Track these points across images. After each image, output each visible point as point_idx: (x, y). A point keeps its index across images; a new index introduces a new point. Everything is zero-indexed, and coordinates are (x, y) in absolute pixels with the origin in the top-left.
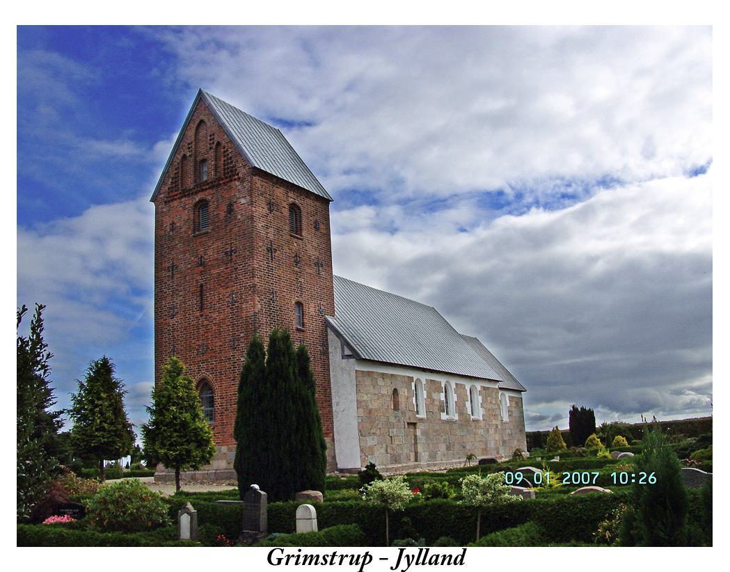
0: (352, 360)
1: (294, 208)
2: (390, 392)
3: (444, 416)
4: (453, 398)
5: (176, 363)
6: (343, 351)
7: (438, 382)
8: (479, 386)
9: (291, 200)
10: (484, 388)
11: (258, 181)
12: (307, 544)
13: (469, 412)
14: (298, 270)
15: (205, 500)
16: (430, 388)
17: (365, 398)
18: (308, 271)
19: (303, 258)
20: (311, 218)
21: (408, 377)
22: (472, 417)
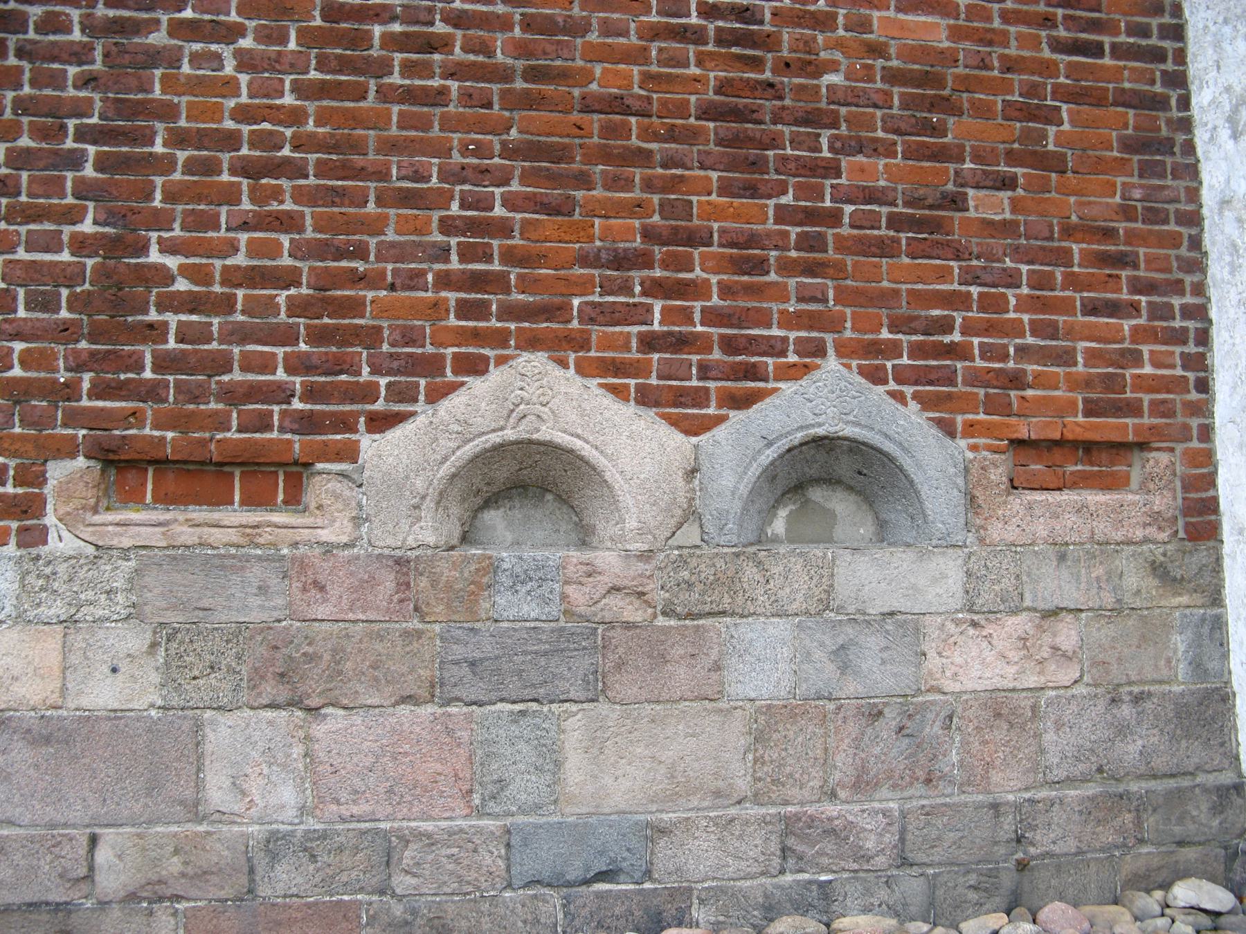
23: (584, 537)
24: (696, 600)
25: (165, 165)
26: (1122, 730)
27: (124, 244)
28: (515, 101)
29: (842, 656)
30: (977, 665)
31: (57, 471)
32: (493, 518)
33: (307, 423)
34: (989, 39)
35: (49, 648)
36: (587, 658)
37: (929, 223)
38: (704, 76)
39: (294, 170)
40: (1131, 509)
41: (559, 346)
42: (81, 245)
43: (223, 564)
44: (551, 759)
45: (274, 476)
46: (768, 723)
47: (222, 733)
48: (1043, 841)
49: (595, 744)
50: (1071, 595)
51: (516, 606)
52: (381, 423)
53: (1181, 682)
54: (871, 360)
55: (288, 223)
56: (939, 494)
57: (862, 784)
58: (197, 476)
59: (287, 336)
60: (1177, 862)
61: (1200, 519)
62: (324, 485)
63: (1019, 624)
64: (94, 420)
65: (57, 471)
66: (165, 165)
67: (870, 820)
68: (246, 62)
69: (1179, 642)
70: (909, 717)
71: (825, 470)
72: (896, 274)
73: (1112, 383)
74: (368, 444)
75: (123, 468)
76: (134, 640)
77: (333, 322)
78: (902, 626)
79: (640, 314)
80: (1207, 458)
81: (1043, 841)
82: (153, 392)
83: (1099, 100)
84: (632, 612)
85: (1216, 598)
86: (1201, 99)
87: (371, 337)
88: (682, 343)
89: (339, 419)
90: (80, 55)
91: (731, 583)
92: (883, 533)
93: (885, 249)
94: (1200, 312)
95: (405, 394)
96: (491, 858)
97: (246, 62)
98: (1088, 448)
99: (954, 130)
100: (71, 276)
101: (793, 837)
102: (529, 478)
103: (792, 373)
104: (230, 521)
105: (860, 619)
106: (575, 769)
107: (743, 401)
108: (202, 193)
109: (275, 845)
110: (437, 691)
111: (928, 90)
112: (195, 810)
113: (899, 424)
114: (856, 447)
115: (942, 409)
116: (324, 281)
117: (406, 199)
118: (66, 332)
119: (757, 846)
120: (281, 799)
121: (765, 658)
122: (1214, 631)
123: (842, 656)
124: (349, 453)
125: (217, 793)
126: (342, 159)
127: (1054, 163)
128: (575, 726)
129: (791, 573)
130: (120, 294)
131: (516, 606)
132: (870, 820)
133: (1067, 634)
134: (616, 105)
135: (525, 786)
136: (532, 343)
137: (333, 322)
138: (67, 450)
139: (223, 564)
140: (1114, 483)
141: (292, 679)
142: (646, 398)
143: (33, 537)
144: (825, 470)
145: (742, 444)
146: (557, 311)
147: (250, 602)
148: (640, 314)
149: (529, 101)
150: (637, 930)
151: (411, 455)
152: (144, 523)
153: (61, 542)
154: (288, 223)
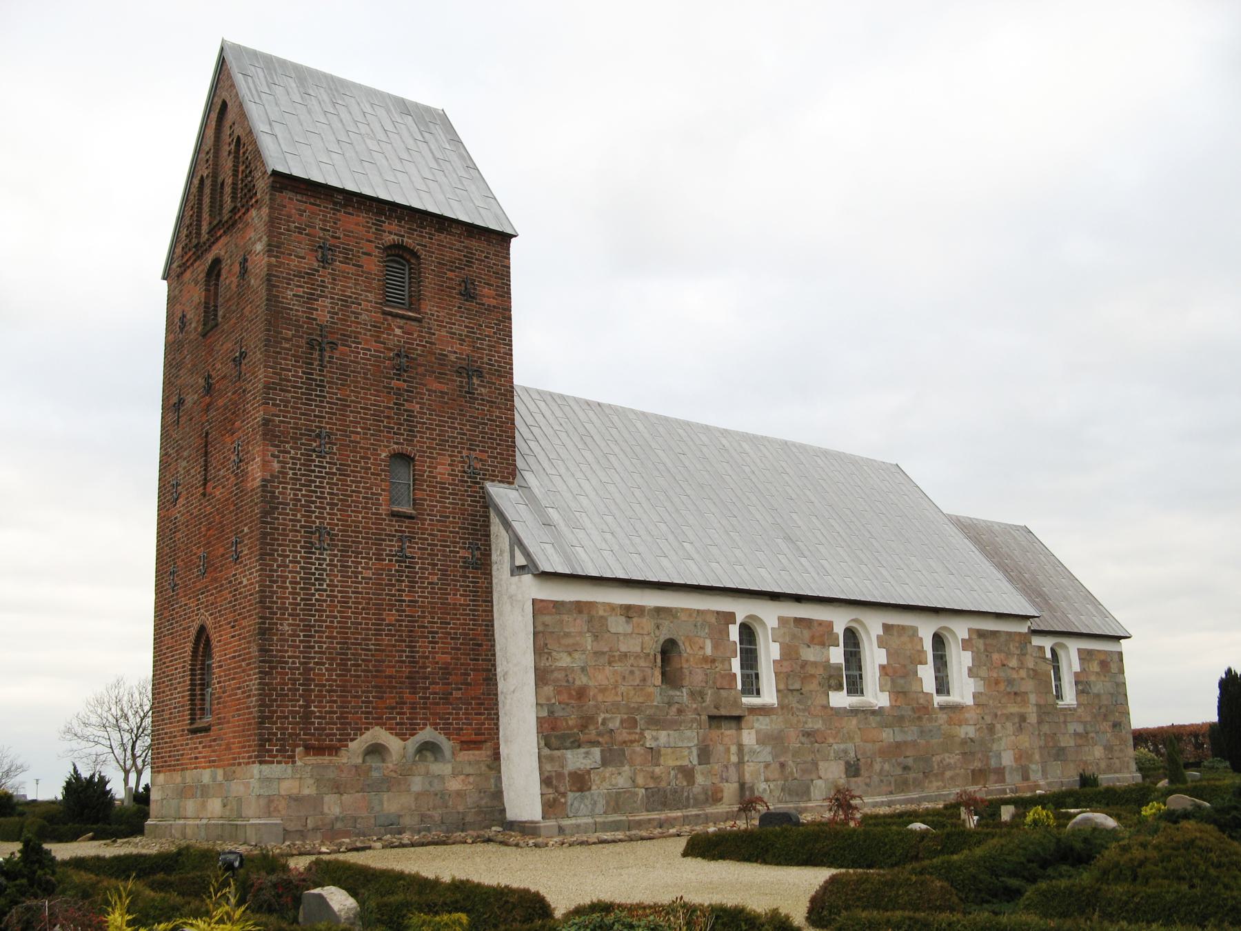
0: (527, 578)
1: (398, 254)
2: (653, 647)
3: (840, 699)
4: (874, 657)
5: (913, 869)
6: (512, 557)
7: (820, 623)
8: (960, 629)
9: (390, 239)
10: (981, 634)
11: (291, 202)
12: (168, 641)
13: (929, 685)
14: (405, 385)
15: (125, 750)
16: (794, 636)
17: (564, 661)
18: (436, 386)
19: (421, 360)
20: (449, 274)
21: (718, 613)
22: (938, 700)
23: (384, 761)
24: (405, 773)
25: (313, 690)
26: (482, 798)
27: (307, 706)
28: (374, 677)
29: (431, 784)
30: (455, 785)
31: (298, 750)
32: (368, 758)
33: (340, 740)
34: (458, 659)
35: (297, 783)
36: (387, 784)
37: (446, 698)
38: (406, 670)
39: (336, 691)
40: (483, 754)
41: (382, 725)
42: (300, 706)
43: (327, 767)
44: (381, 803)
45: (334, 750)
46: (418, 796)
47: (327, 798)
48: (467, 819)
49: (389, 800)
50: (471, 771)
51: (375, 774)
52: (352, 740)
53: (493, 789)
54: (435, 726)
55: (335, 702)
56: (448, 753)
57: (434, 808)
58: (319, 750)
59: (335, 724)
60: (1131, 860)
61: (496, 756)
62: (343, 752)
63: (462, 777)
64: (304, 740)
65: (298, 750)
66: (313, 690)
67: (437, 815)
68: (327, 670)
69: (492, 781)
70: (443, 795)
71: (429, 748)
72: (440, 709)
73: (480, 729)
74: (350, 744)
75: (308, 749)
76: (311, 781)
77: (343, 721)
78: (441, 778)
79: (395, 718)
80: (498, 744)
81: (467, 819)
82: (313, 735)
83: (478, 670)
84: (394, 775)
85: (500, 772)
86: (498, 670)
87: (350, 724)
88: (402, 724)
89: (345, 739)
90: (298, 669)
91: (410, 769)
92: (436, 760)
93: (438, 704)
94: (497, 714)
95: (355, 734)
96: (373, 821)
97: (327, 670)
98: (475, 742)
99: (451, 679)
100: (298, 712)
101: (423, 818)
102: (377, 750)
103: (421, 729)
104: (326, 759)
105: (434, 776)
106: (386, 804)
107: (412, 735)
108: (320, 696)
109: (337, 819)
110: (362, 790)
111: (446, 670)
112: (322, 813)
113: (441, 739)
114: (433, 743)
115: (448, 735)
116: (342, 713)
117: (355, 697)
118: (298, 723)
119: (417, 819)
120: (336, 811)
121: (417, 784)
122: (499, 779)
123: (431, 784)
124: (347, 746)
125: (326, 810)
126: (344, 688)
127: (470, 684)
128: (385, 796)
129: (421, 768)
130: (307, 716)
131: (375, 774)
132: (437, 815)
133: (471, 779)
134: (391, 677)
135: (377, 808)
136: (377, 724)
137: (343, 721)
138: (299, 746)
139: (327, 767)
140: (479, 749)
141: (338, 788)
142: (397, 735)
143: (294, 762)
144: (429, 748)
145: (413, 743)
146: (381, 718)
147: (331, 774)
148: (395, 718)
149: (376, 676)
150: (648, 928)
151: (357, 746)
152: (312, 759)
153: (299, 763)
154: (335, 702)
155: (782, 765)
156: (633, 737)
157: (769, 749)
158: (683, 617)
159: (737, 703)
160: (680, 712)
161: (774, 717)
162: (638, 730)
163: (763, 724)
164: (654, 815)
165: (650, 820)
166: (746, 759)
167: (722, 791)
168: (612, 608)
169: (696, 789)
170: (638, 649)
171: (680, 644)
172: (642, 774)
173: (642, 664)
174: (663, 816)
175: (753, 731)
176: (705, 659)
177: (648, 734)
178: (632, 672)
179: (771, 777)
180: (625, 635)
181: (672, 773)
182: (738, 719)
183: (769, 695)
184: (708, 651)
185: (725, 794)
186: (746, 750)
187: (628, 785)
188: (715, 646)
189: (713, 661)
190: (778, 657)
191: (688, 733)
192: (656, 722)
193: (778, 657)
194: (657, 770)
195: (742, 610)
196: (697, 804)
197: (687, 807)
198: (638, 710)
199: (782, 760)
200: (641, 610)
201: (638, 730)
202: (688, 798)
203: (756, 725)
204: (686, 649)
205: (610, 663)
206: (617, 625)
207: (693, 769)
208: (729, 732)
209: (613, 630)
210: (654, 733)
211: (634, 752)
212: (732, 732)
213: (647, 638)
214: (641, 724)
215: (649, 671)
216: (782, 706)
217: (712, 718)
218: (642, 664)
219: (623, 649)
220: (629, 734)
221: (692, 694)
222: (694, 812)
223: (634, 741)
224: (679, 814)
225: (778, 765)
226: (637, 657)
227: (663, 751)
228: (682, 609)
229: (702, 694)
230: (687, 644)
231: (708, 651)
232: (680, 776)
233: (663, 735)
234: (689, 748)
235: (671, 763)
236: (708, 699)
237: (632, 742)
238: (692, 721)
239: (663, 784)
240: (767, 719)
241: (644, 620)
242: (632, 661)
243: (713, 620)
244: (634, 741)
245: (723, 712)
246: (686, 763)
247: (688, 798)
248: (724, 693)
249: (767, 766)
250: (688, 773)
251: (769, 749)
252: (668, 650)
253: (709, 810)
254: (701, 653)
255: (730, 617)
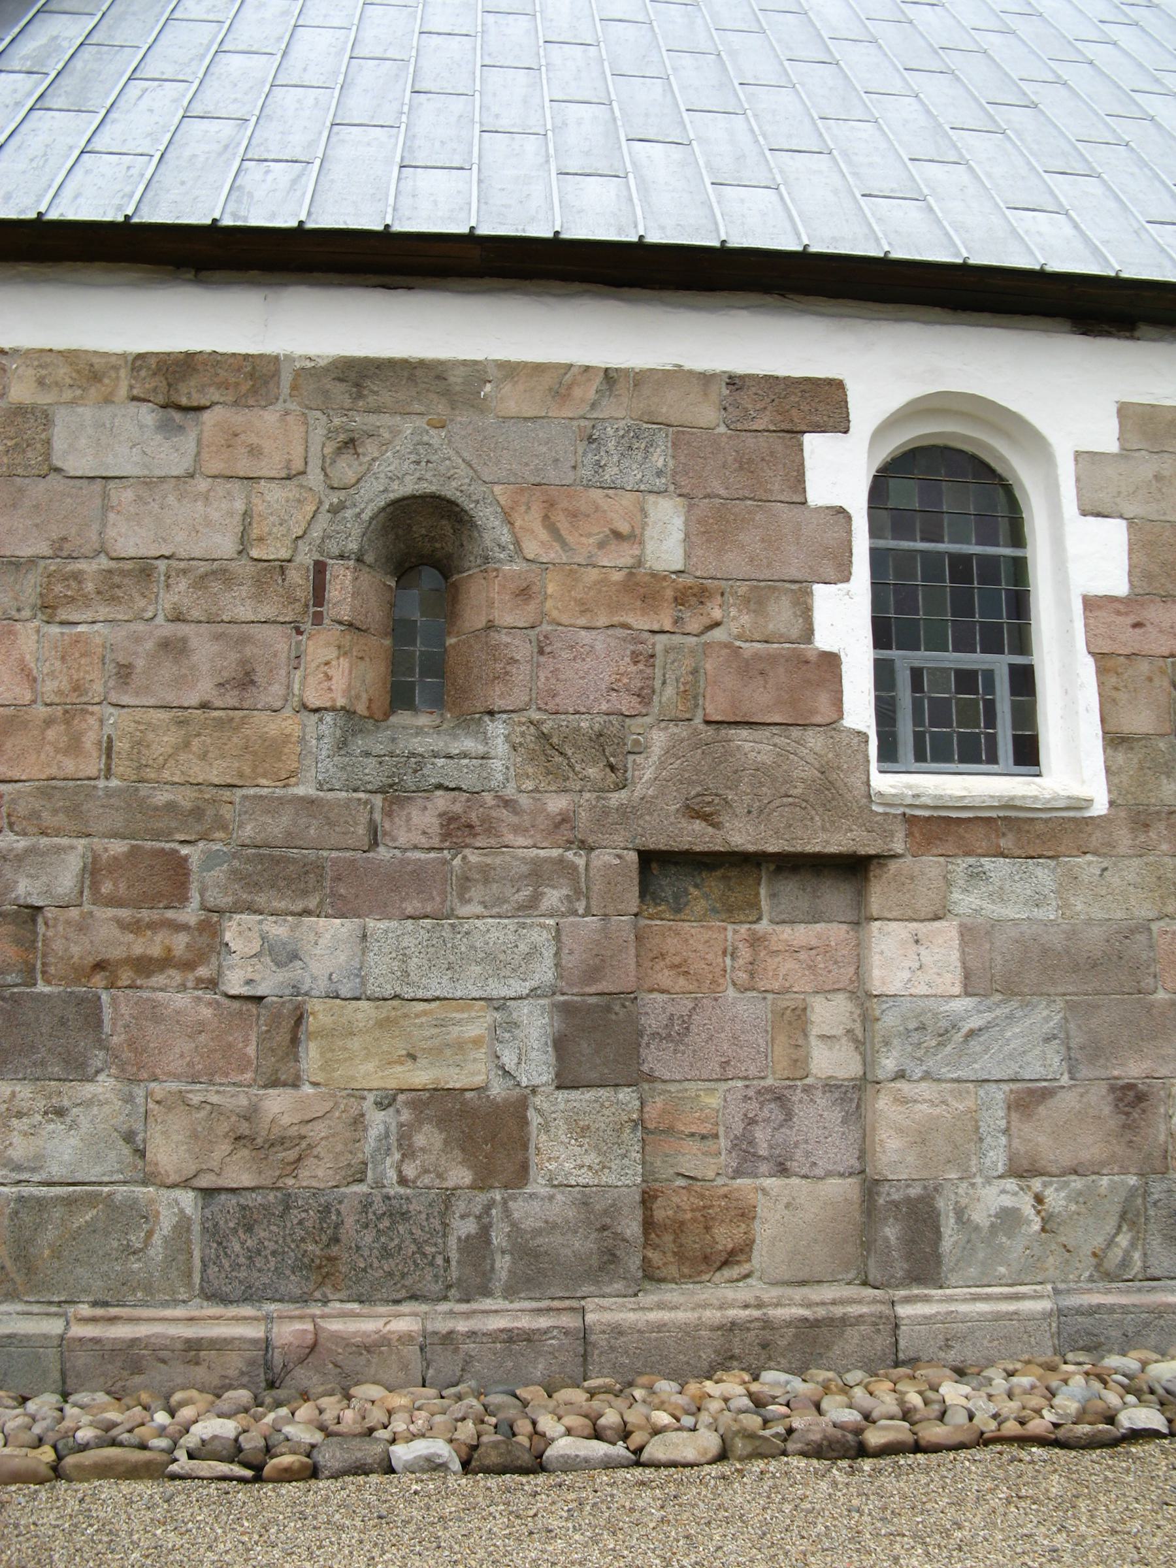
21: (735, 382)
53: (793, 1165)
155: (1132, 1099)
156: (153, 946)
157: (1045, 1016)
158: (513, 400)
159: (832, 791)
160: (456, 830)
161: (1088, 865)
162: (190, 914)
163: (1014, 896)
164: (238, 1325)
165: (193, 1349)
166: (889, 1064)
167: (746, 1214)
168: (88, 372)
169: (535, 1206)
170: (224, 544)
171: (486, 516)
172: (178, 1123)
173: (240, 606)
174: (292, 1331)
175: (946, 933)
176: (643, 587)
177: (240, 934)
178: (173, 648)
179: (1051, 1152)
180: (149, 482)
181: (378, 1121)
182: (854, 868)
183: (1074, 766)
184: (667, 541)
185: (764, 1231)
186: (890, 1021)
187: (107, 1166)
188: (712, 527)
189: (691, 594)
190: (1118, 585)
191: (494, 932)
192: (286, 875)
193: (1118, 585)
194: (278, 1105)
195: (888, 373)
196: (535, 1271)
197: (476, 1286)
198: (200, 818)
199: (1133, 1070)
200: (255, 377)
201: (190, 914)
202: (478, 1247)
203: (966, 901)
204: (512, 540)
205: (47, 608)
206: (109, 441)
207: (517, 1110)
208: (794, 933)
209: (76, 465)
210: (278, 930)
211: (154, 1012)
212: (836, 932)
213: (276, 495)
214: (209, 882)
215: (279, 641)
216: (1136, 814)
217: (655, 864)
218: (240, 606)
219: (131, 539)
220: (135, 927)
221: (547, 750)
222: (500, 1315)
223: (165, 962)
224: (404, 1322)
225: (1099, 1099)
226: (214, 575)
227: (320, 1015)
228: (511, 370)
229: (611, 751)
230: (530, 520)
231: (667, 541)
232: (427, 1137)
233: (328, 944)
234: (499, 1004)
235: (370, 1074)
236: (646, 773)
237: (145, 966)
238: (538, 874)
239: (318, 1173)
240: (1043, 874)
241: (270, 417)
242: (179, 593)
243: (707, 414)
244: (165, 962)
245: (740, 835)
246: (470, 1073)
247: (478, 1247)
248: (752, 747)
249: (1029, 1099)
250: (491, 1134)
251: (1045, 1016)
252: (424, 546)
253: (610, 1311)
254: (620, 557)
255: (824, 404)
